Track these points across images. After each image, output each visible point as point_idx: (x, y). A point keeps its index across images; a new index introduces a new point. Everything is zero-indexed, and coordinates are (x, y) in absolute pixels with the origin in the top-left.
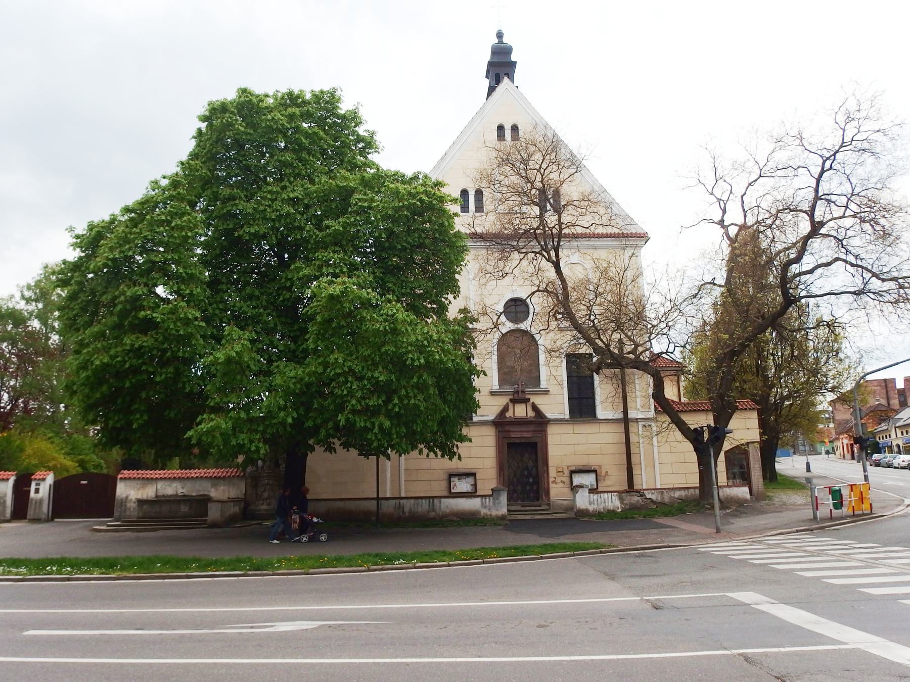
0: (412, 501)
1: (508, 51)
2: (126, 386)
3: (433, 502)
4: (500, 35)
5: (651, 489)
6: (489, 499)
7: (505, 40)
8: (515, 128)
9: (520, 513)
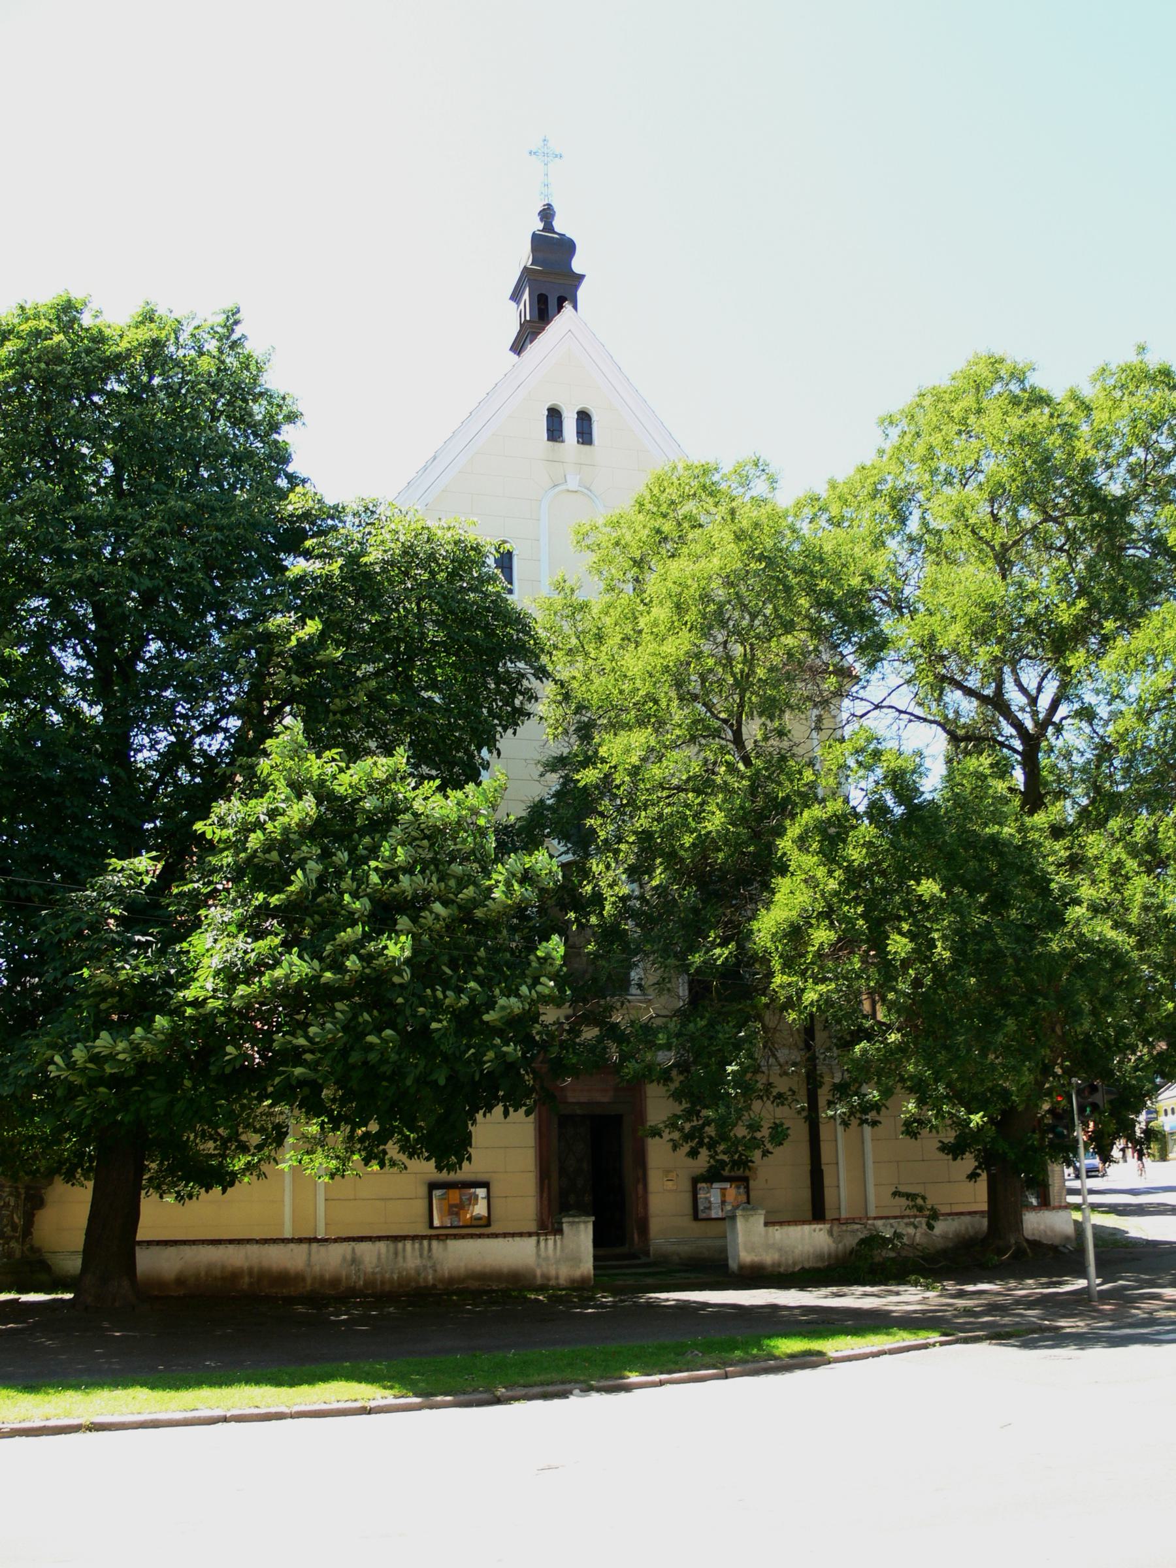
0: (382, 1246)
1: (567, 247)
2: (486, 1017)
3: (430, 1245)
4: (547, 214)
5: (887, 1218)
6: (421, 1244)
7: (559, 225)
8: (584, 418)
9: (634, 1270)
